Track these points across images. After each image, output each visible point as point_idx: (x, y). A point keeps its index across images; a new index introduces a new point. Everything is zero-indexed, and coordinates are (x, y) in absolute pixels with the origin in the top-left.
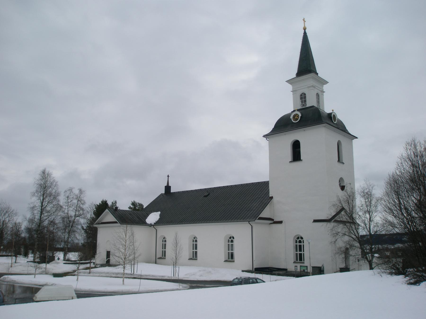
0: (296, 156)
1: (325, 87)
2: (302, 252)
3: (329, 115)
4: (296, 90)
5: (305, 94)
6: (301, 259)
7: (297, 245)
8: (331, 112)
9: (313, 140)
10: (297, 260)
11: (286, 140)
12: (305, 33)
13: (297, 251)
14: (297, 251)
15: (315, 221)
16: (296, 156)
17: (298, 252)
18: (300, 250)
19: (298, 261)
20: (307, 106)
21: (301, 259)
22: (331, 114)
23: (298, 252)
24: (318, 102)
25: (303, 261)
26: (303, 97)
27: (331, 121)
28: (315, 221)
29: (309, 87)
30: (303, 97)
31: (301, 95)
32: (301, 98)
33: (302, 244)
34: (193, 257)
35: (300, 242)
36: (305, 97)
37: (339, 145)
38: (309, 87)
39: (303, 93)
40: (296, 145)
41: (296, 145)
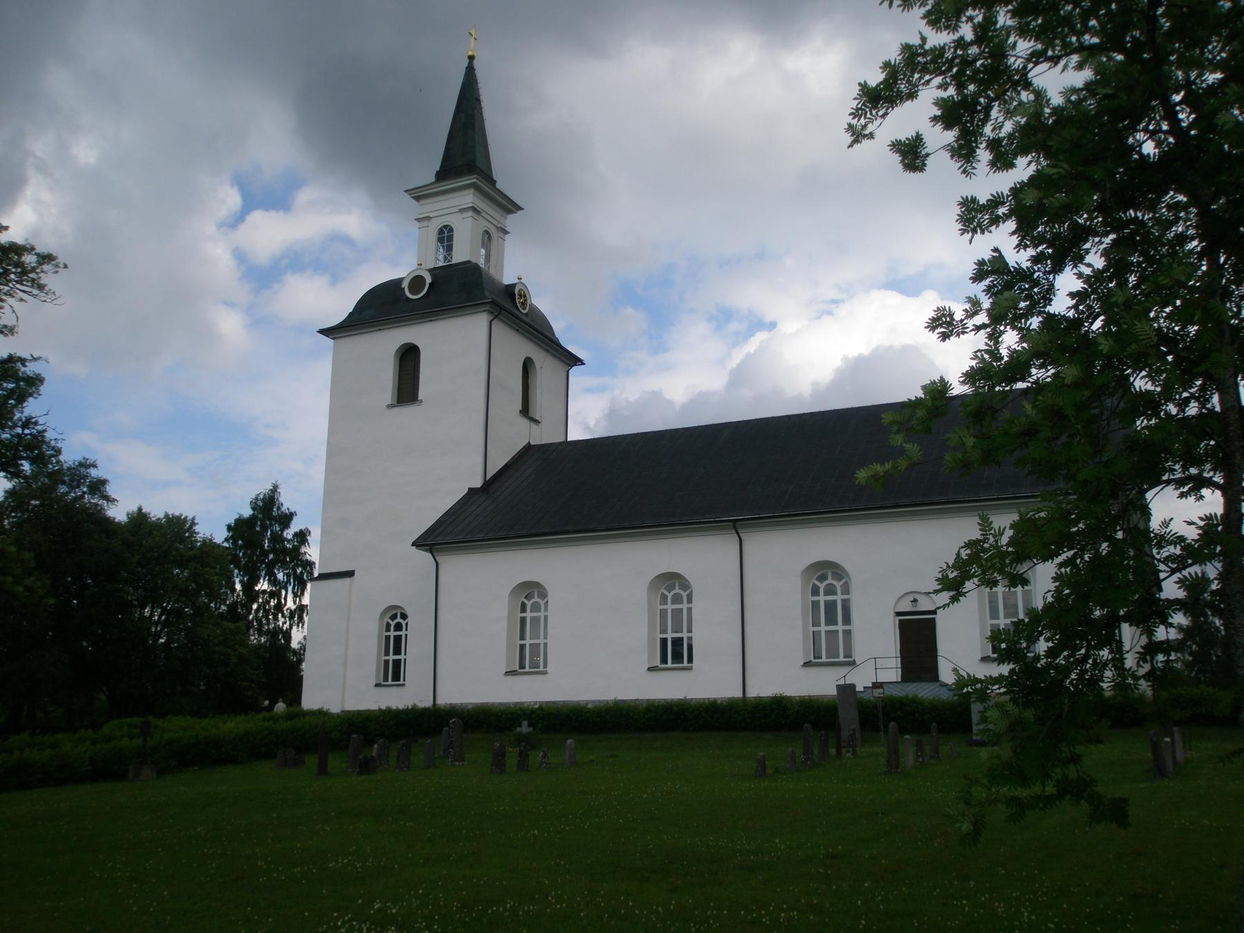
0: (407, 389)
1: (511, 221)
2: (402, 657)
3: (509, 291)
4: (429, 218)
5: (451, 230)
6: (677, 657)
7: (388, 638)
8: (516, 281)
9: (457, 347)
10: (386, 679)
11: (388, 341)
12: (470, 72)
13: (387, 653)
14: (816, 623)
15: (350, 574)
16: (407, 389)
17: (823, 628)
18: (397, 651)
19: (670, 664)
20: (454, 262)
21: (396, 677)
22: (514, 286)
23: (392, 657)
24: (488, 257)
25: (685, 664)
26: (446, 236)
27: (510, 307)
28: (350, 574)
29: (462, 211)
30: (446, 236)
31: (441, 231)
32: (441, 240)
33: (403, 633)
34: (522, 666)
35: (677, 599)
36: (451, 238)
37: (527, 366)
38: (462, 211)
39: (446, 226)
40: (409, 357)
41: (409, 357)
